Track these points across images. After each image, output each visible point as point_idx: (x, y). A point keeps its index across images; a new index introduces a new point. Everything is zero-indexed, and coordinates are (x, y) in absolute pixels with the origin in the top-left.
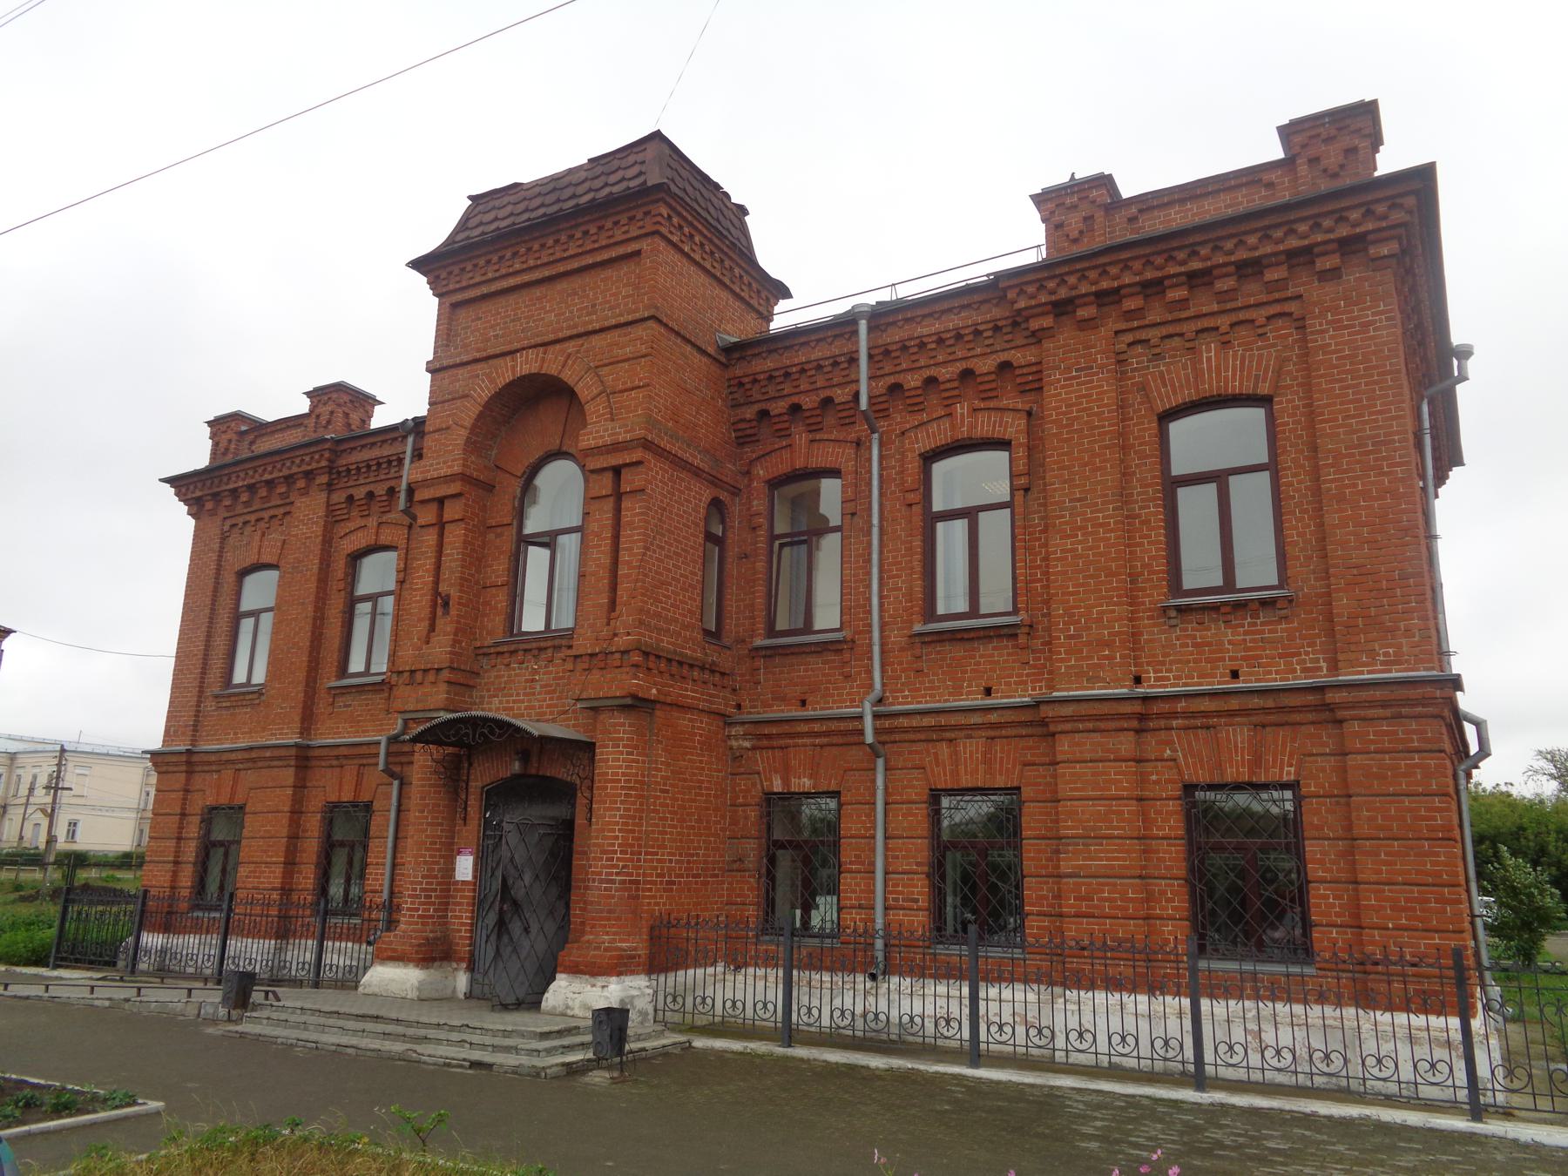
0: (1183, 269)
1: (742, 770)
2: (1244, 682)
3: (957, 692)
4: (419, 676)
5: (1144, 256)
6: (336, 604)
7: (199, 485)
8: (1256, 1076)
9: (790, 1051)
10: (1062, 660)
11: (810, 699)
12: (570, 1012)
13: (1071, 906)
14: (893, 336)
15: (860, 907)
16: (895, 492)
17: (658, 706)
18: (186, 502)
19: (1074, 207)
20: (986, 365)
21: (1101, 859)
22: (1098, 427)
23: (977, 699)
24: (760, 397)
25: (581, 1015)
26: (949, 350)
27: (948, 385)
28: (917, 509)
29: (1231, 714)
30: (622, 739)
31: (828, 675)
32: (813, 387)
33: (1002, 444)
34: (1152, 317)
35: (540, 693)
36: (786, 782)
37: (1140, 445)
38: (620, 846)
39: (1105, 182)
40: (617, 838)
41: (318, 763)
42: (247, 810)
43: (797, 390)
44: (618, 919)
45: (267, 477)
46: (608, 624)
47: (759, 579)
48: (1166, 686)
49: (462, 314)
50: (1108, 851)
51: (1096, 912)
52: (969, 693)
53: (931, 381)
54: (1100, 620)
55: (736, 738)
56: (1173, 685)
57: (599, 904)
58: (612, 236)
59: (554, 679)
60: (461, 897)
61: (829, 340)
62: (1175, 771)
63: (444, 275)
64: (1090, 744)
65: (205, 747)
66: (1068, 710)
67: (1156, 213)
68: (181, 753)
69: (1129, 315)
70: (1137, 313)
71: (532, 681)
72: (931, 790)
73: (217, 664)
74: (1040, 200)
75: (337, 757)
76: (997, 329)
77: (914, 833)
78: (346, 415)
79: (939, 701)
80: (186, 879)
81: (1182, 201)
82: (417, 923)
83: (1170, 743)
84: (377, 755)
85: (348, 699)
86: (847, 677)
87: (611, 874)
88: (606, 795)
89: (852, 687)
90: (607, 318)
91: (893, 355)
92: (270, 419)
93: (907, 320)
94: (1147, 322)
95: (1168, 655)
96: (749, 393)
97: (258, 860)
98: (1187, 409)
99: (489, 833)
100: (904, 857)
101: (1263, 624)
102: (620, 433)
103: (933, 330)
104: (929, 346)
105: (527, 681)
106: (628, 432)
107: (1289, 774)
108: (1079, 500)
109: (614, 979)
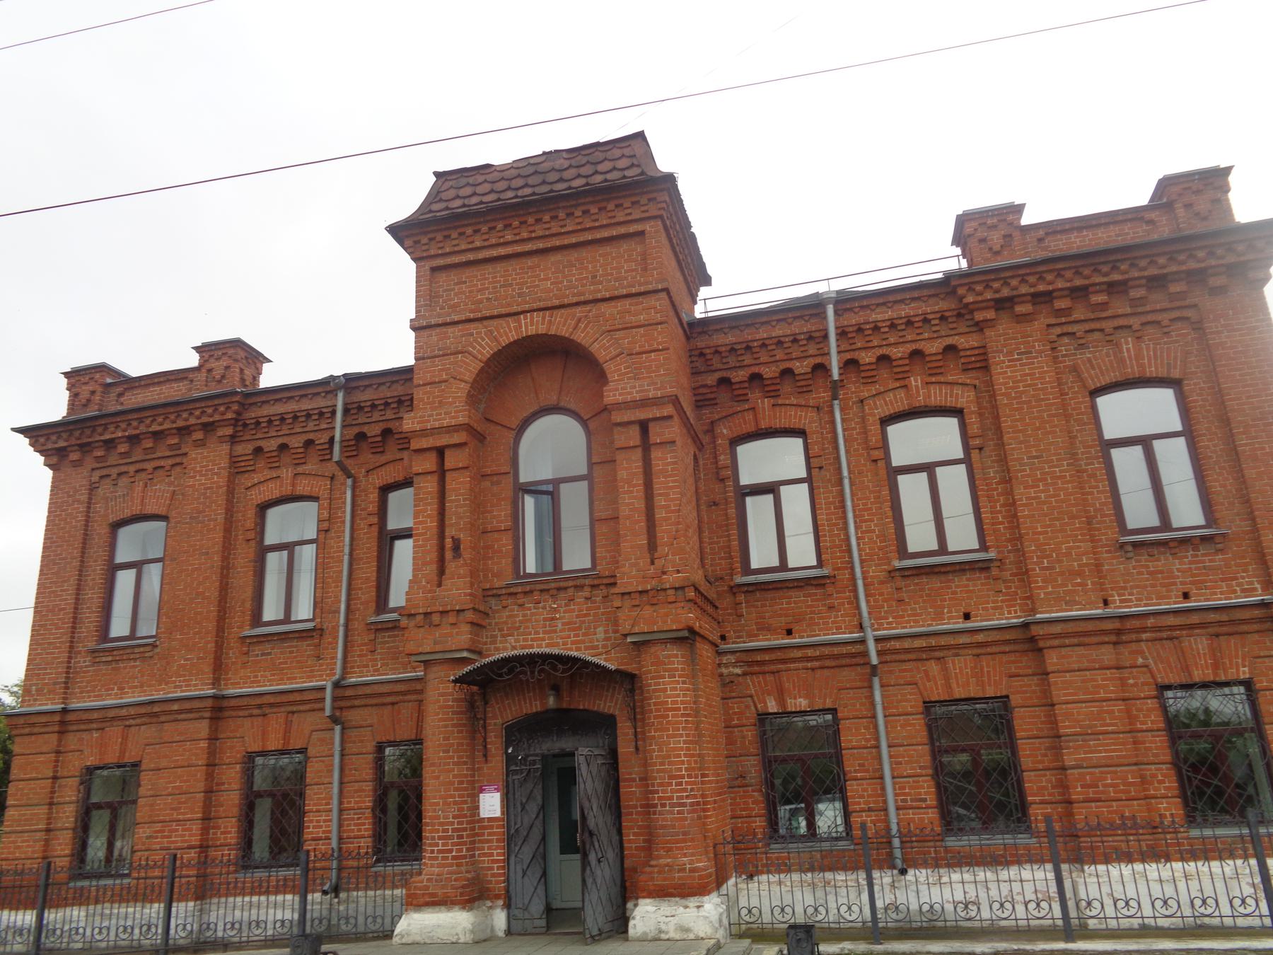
0: (1105, 279)
1: (734, 694)
2: (1195, 601)
3: (939, 617)
4: (436, 619)
5: (1075, 267)
6: (243, 556)
7: (65, 435)
8: (1113, 924)
10: (1040, 588)
11: (795, 628)
12: (663, 936)
13: (1078, 793)
14: (852, 319)
15: (870, 810)
16: (858, 450)
18: (41, 452)
19: (994, 227)
20: (933, 348)
21: (1100, 752)
22: (1043, 399)
23: (958, 623)
24: (720, 366)
25: (677, 937)
26: (901, 334)
27: (901, 362)
29: (1192, 627)
30: (677, 670)
31: (811, 606)
32: (773, 359)
34: (1076, 315)
35: (561, 631)
36: (781, 701)
37: (1078, 414)
38: (687, 769)
40: (683, 762)
41: (233, 713)
42: (143, 767)
43: (757, 362)
44: (692, 840)
45: (155, 428)
46: (653, 563)
47: (732, 524)
48: (1130, 607)
49: (442, 277)
50: (1107, 745)
51: (1103, 797)
52: (950, 618)
53: (883, 359)
54: (1068, 554)
55: (726, 665)
56: (1136, 606)
57: (673, 827)
58: (630, 214)
59: (578, 616)
60: (489, 834)
62: (1149, 675)
63: (425, 240)
64: (1076, 656)
65: (75, 705)
66: (1057, 629)
67: (1059, 237)
68: (53, 713)
69: (1059, 313)
70: (1066, 312)
71: (552, 619)
72: (924, 702)
73: (90, 618)
75: (260, 706)
76: (943, 318)
77: (914, 741)
78: (242, 370)
79: (923, 626)
80: (63, 847)
81: (1080, 229)
82: (451, 865)
83: (1141, 653)
84: (323, 699)
85: (267, 647)
86: (831, 607)
87: (682, 798)
88: (668, 723)
89: (836, 617)
90: (582, 294)
91: (850, 335)
92: (134, 375)
93: (862, 307)
94: (108, 464)
95: (1128, 581)
96: (709, 363)
97: (167, 818)
98: (1140, 382)
99: (513, 768)
100: (907, 763)
101: (1204, 555)
102: (649, 391)
103: (937, 308)
104: (882, 330)
105: (545, 620)
106: (659, 389)
107: (1244, 673)
108: (1037, 457)
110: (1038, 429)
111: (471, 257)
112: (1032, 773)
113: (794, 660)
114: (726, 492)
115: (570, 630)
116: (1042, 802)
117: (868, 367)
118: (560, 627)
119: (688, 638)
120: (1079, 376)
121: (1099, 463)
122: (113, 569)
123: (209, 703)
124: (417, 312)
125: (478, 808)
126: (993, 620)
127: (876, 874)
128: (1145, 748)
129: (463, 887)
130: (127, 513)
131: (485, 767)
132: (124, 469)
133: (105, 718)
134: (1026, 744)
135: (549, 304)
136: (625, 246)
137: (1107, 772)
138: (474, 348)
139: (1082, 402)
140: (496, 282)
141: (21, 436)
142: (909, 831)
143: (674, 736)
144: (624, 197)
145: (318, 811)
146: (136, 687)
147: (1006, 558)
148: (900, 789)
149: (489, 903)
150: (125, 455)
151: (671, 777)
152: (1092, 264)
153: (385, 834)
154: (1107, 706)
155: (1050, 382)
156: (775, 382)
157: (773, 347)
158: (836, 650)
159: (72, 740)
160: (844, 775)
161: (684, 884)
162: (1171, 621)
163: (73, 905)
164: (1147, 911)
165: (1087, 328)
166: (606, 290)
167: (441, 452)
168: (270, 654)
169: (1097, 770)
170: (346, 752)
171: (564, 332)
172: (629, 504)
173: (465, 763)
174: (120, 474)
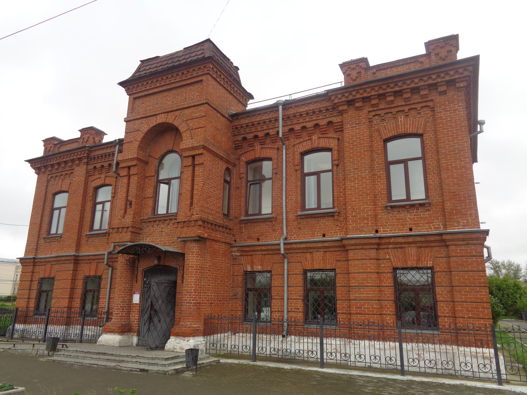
0: (392, 90)
1: (236, 263)
2: (414, 232)
3: (313, 235)
4: (120, 230)
5: (379, 85)
6: (89, 205)
9: (255, 363)
10: (350, 224)
12: (175, 350)
13: (354, 310)
15: (279, 311)
16: (291, 166)
17: (207, 240)
18: (34, 169)
19: (354, 69)
20: (323, 122)
23: (320, 238)
25: (179, 351)
27: (310, 129)
28: (299, 172)
30: (194, 252)
31: (268, 230)
33: (329, 150)
34: (381, 107)
36: (252, 267)
38: (194, 290)
39: (364, 60)
45: (65, 160)
46: (190, 211)
49: (137, 101)
52: (317, 236)
55: (234, 252)
57: (186, 311)
59: (170, 231)
60: (135, 309)
61: (320, 102)
64: (360, 254)
66: (353, 242)
69: (373, 106)
70: (376, 105)
74: (342, 66)
75: (89, 260)
76: (327, 110)
77: (298, 285)
78: (94, 138)
79: (307, 239)
81: (391, 67)
83: (388, 253)
84: (104, 259)
86: (274, 230)
89: (276, 234)
90: (179, 106)
91: (291, 118)
92: (65, 140)
93: (296, 106)
94: (412, 102)
95: (388, 223)
97: (59, 297)
99: (145, 286)
101: (420, 212)
102: (194, 143)
104: (303, 116)
107: (430, 264)
108: (356, 169)
109: (192, 338)
110: (359, 157)
111: (146, 93)
112: (340, 301)
113: (258, 251)
114: (242, 183)
115: (167, 236)
116: (342, 313)
117: (298, 132)
118: (164, 234)
119: (200, 240)
120: (380, 133)
121: (383, 171)
122: (53, 210)
123: (73, 258)
124: (128, 115)
125: (132, 299)
126: (333, 237)
127: (404, 345)
128: (384, 294)
129: (119, 327)
130: (57, 190)
131: (136, 284)
132: (57, 174)
133: (46, 261)
134: (339, 289)
135: (168, 110)
136: (197, 86)
137: (367, 303)
138: (142, 128)
139: (380, 145)
140: (154, 103)
141: (28, 163)
142: (383, 325)
143: (190, 277)
144: (195, 66)
145: (103, 298)
146: (55, 251)
147: (342, 211)
148: (290, 304)
149: (132, 334)
150: (57, 169)
151: (187, 292)
152: (402, 80)
153: (247, 313)
154: (370, 275)
155: (366, 136)
156: (263, 138)
157: (262, 124)
158: (272, 247)
159: (37, 269)
160: (271, 297)
161: (185, 332)
162: (401, 240)
163: (34, 324)
164: (368, 360)
165: (386, 112)
166: (187, 104)
167: (129, 167)
168: (94, 241)
169: (362, 302)
170: (113, 278)
171: (170, 121)
172: (186, 188)
173: (127, 283)
174: (61, 175)
